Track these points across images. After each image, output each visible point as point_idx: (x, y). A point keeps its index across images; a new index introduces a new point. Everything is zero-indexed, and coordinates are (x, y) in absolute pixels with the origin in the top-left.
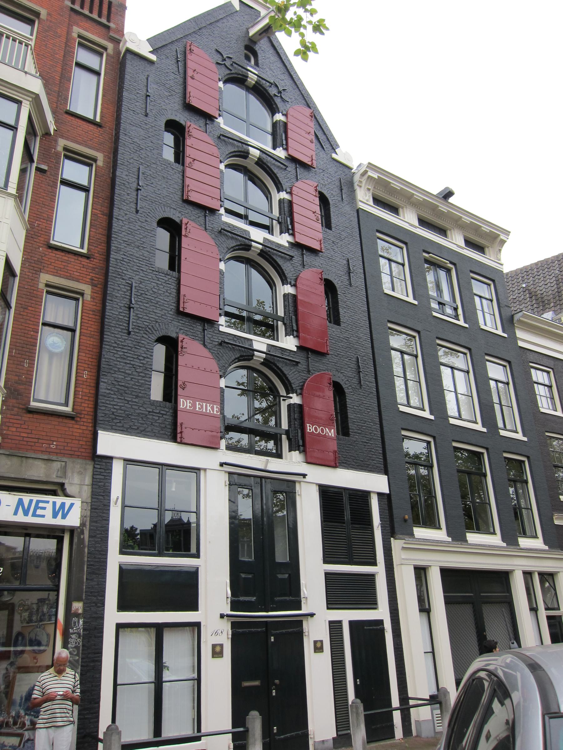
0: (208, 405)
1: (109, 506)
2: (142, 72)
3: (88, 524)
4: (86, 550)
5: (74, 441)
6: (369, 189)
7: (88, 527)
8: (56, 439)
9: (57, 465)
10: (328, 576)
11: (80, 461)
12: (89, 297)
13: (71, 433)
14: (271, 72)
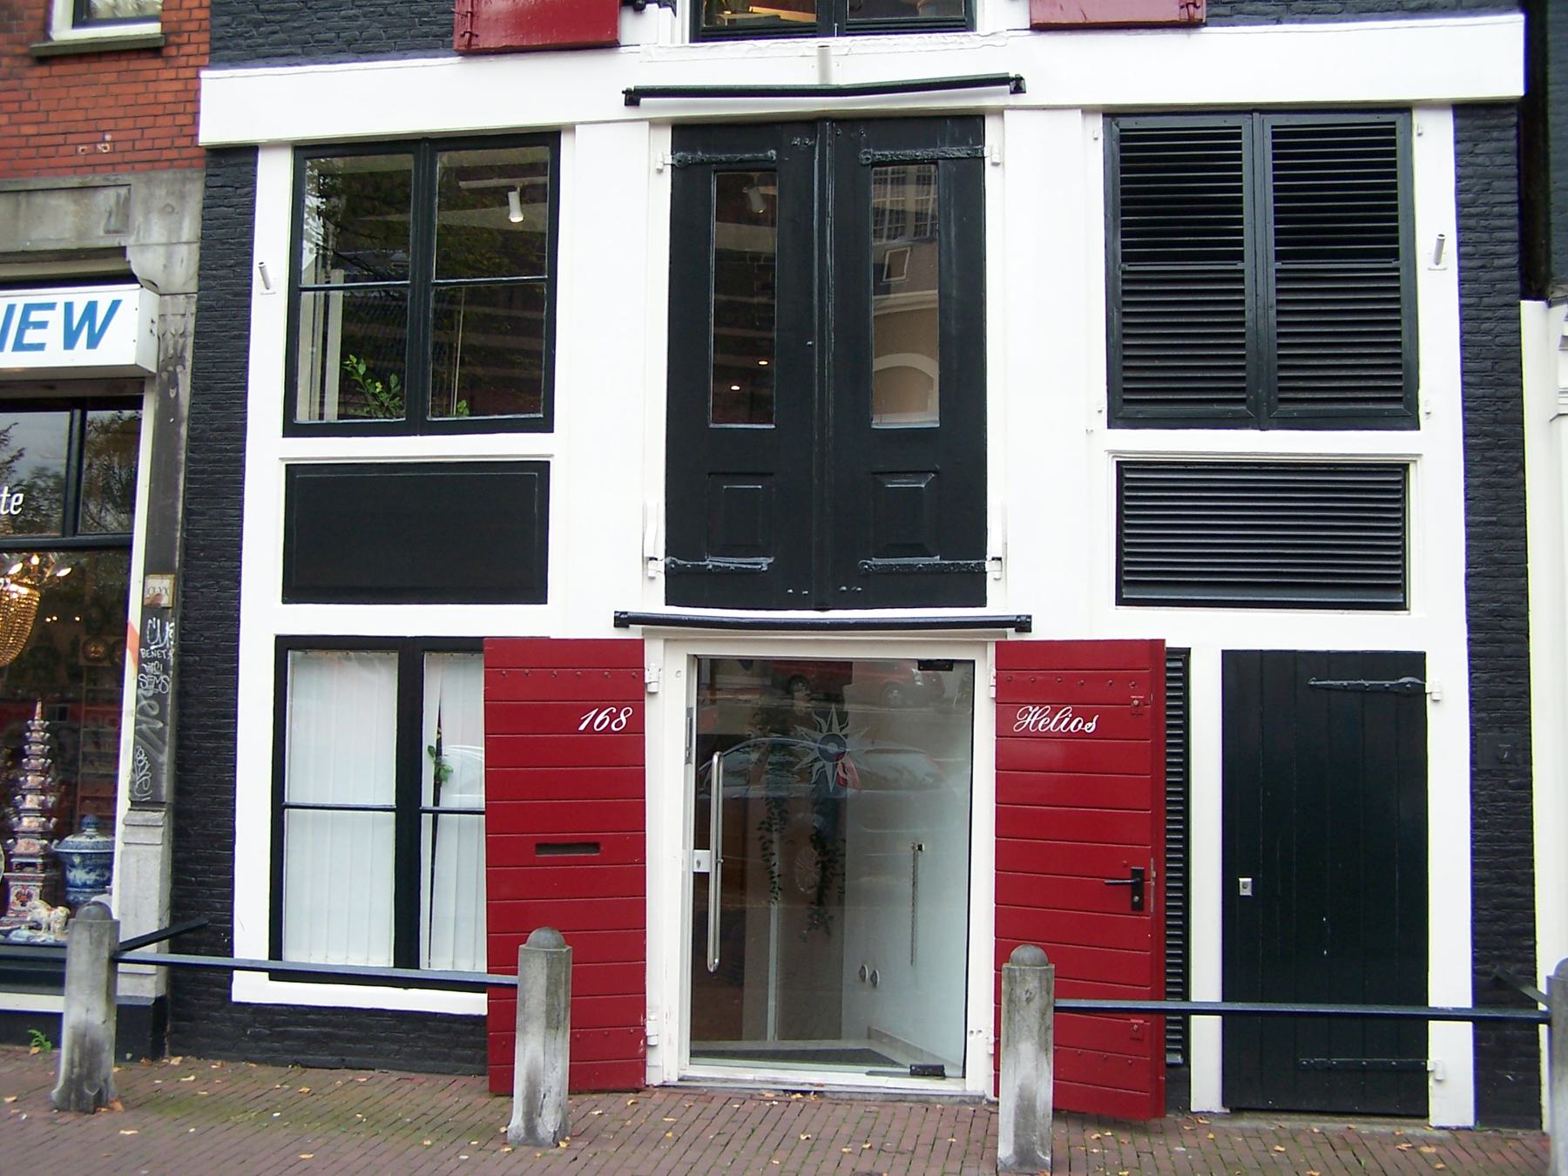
1: (249, 295)
3: (189, 355)
4: (184, 431)
5: (160, 121)
7: (189, 364)
8: (110, 124)
9: (106, 200)
10: (1129, 473)
11: (167, 175)
13: (151, 98)
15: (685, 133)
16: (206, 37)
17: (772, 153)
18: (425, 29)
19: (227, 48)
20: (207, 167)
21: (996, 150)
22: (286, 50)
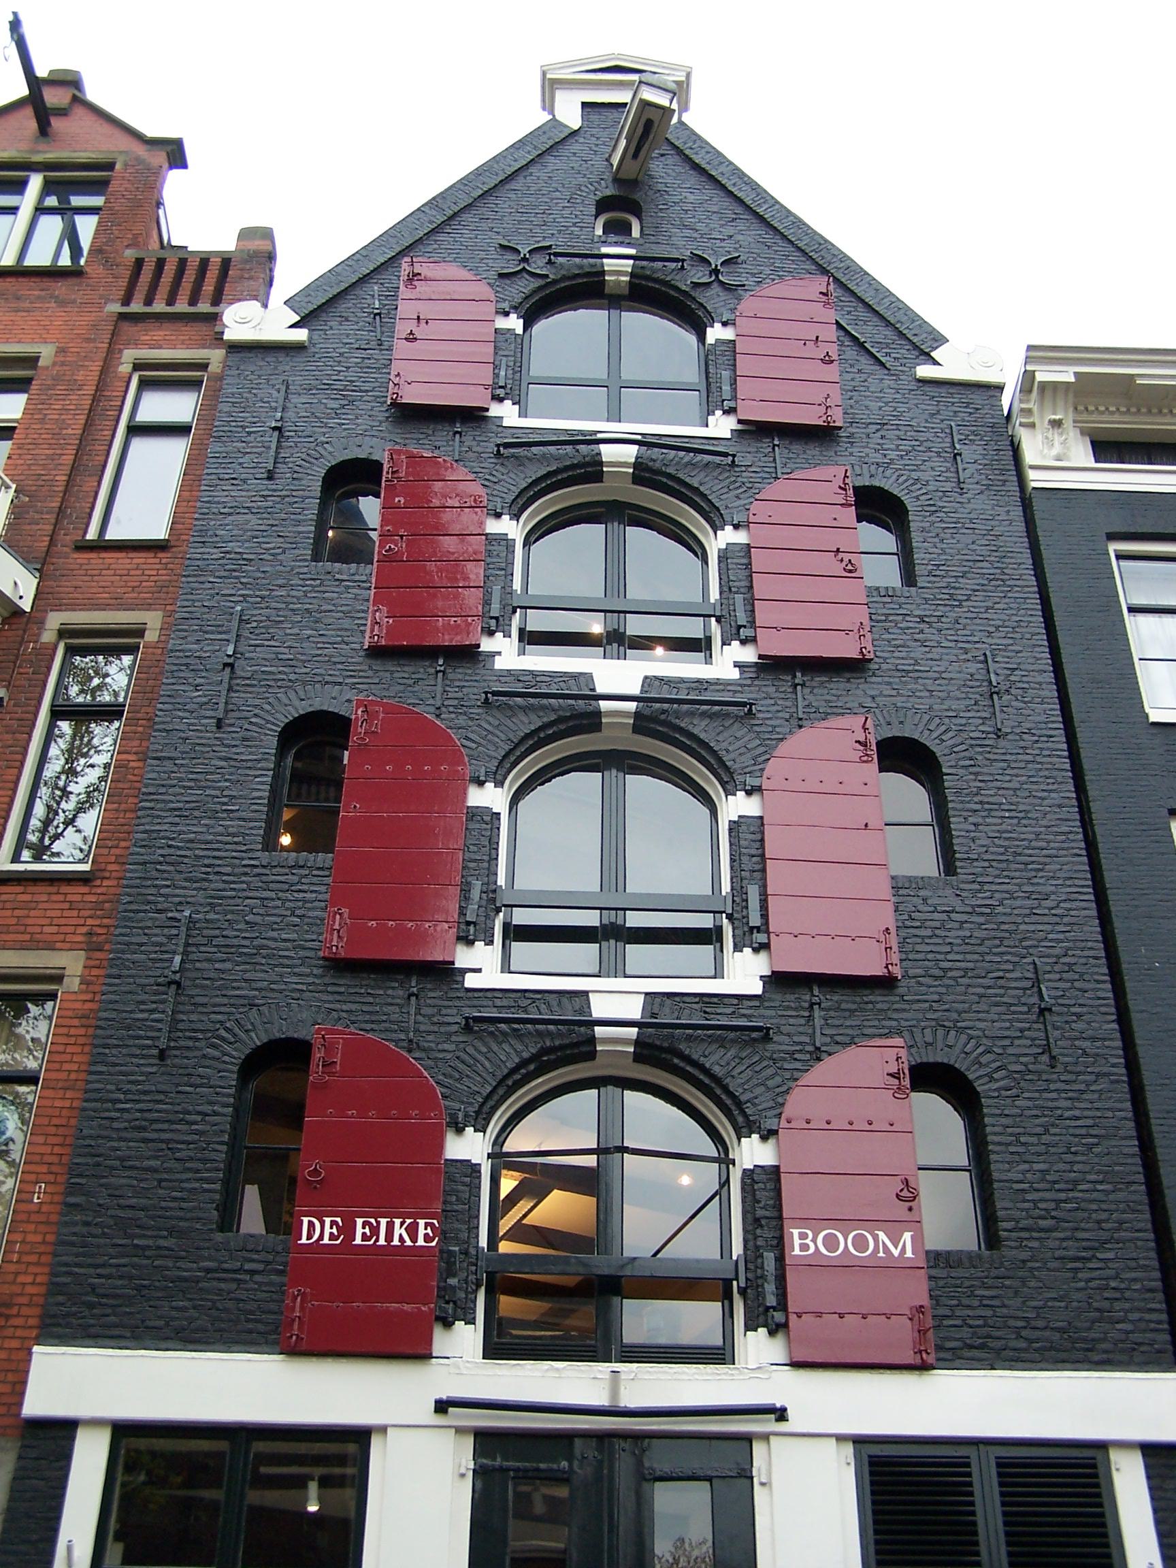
0: (397, 1222)
2: (268, 380)
6: (1056, 424)
12: (77, 981)
14: (687, 232)
15: (485, 1440)
16: (36, 1311)
17: (564, 1464)
18: (250, 1326)
19: (59, 1325)
20: (23, 1437)
21: (764, 1471)
22: (116, 1332)
